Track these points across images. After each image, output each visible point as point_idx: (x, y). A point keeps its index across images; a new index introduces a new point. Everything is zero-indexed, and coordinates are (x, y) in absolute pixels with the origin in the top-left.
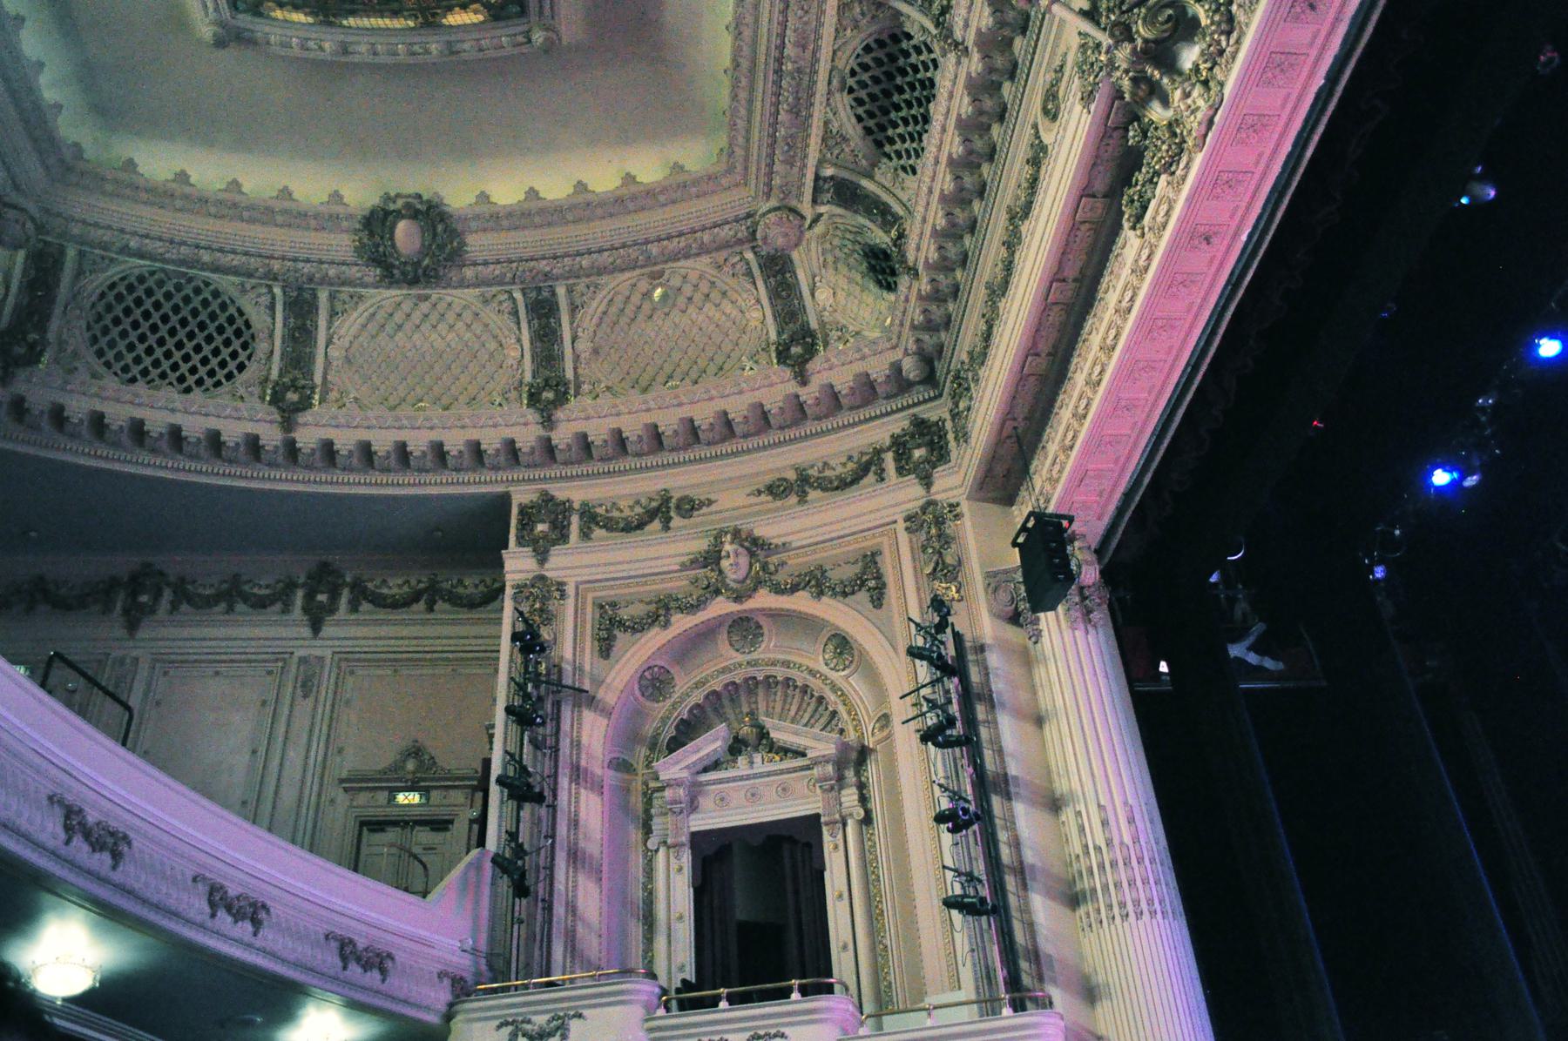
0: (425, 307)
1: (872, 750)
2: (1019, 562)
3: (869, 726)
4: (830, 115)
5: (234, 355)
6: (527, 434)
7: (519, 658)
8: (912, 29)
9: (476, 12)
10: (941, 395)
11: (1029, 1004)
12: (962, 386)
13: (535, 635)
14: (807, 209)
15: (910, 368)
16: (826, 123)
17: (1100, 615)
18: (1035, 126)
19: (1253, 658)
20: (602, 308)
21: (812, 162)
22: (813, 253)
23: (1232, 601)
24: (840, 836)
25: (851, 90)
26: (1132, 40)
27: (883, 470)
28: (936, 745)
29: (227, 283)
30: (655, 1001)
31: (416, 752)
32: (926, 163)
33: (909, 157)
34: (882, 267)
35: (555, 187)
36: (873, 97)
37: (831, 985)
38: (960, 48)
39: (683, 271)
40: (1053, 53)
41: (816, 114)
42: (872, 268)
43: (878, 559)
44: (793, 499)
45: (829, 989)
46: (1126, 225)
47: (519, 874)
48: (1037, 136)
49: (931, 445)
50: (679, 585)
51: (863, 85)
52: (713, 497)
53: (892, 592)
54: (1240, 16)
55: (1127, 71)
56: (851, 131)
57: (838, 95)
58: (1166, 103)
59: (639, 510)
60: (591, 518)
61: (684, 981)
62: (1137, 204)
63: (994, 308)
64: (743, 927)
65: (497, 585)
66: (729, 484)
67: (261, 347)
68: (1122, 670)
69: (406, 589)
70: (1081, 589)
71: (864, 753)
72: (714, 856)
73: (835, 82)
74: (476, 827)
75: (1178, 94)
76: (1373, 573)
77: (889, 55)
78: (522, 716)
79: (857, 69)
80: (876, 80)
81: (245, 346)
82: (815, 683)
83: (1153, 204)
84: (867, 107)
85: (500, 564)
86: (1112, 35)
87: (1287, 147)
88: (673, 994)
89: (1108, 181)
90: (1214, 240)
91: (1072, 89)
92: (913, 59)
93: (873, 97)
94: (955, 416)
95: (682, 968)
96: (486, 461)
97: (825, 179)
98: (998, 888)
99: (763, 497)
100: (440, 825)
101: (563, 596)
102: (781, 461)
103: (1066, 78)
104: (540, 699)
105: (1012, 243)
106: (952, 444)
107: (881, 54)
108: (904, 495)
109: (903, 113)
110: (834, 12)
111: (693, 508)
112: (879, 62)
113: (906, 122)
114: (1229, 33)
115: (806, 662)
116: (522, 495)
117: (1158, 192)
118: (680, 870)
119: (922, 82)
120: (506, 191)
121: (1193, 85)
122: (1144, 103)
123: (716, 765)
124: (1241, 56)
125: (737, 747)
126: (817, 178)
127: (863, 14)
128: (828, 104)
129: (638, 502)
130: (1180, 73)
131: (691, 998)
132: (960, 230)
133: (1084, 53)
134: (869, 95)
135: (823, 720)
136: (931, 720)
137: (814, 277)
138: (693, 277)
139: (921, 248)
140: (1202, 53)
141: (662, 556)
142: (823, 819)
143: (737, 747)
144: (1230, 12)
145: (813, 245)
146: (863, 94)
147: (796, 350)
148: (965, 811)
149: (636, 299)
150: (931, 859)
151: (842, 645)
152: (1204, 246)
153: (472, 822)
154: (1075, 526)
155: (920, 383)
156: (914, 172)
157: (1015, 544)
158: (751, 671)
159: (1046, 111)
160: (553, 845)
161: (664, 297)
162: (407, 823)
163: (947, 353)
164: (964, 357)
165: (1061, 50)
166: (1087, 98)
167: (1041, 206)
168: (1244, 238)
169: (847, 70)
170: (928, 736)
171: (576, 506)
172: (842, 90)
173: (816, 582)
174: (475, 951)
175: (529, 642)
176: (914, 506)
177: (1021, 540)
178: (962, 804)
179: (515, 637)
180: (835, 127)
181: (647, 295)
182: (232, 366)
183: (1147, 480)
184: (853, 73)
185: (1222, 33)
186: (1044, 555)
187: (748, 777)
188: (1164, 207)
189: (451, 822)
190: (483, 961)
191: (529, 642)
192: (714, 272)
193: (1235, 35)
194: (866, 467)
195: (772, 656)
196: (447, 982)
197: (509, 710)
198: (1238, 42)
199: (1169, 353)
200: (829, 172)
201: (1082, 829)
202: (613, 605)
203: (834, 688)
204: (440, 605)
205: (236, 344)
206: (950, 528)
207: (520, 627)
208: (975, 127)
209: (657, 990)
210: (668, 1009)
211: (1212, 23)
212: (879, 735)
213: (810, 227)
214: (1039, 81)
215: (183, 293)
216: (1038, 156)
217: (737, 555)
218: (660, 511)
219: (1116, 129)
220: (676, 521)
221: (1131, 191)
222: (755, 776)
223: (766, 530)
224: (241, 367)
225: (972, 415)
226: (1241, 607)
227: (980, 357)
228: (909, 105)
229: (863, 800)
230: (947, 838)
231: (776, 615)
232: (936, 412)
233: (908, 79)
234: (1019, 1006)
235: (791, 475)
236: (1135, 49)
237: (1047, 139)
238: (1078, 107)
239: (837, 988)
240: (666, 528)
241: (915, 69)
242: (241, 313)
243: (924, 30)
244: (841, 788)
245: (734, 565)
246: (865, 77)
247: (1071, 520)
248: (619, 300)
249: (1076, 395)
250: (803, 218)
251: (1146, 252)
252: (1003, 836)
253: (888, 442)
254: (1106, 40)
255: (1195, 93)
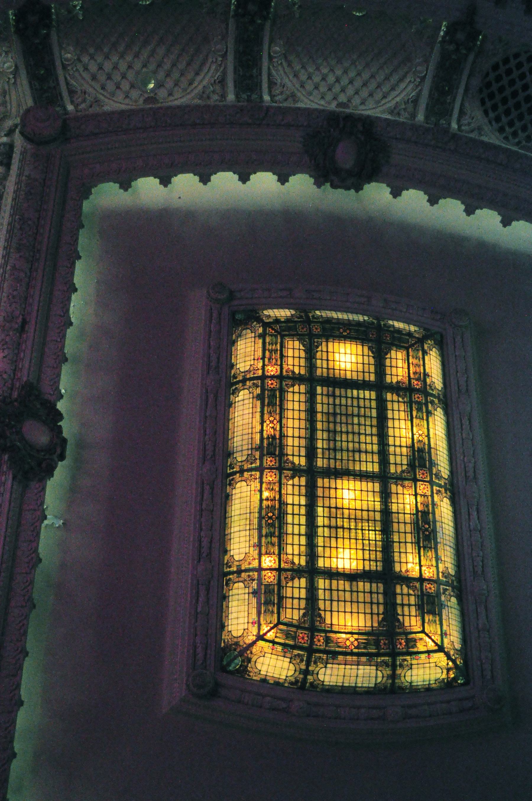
0: (342, 98)
5: (498, 79)
9: (269, 316)
20: (394, 94)
22: (14, 104)
29: (21, 111)
39: (127, 101)
67: (476, 82)
81: (488, 85)
137: (15, 83)
138: (120, 96)
145: (14, 110)
149: (169, 83)
181: (159, 85)
182: (502, 69)
205: (495, 87)
215: (513, 129)
224: (496, 67)
242: (486, 113)
248: (378, 95)
250: (22, 133)
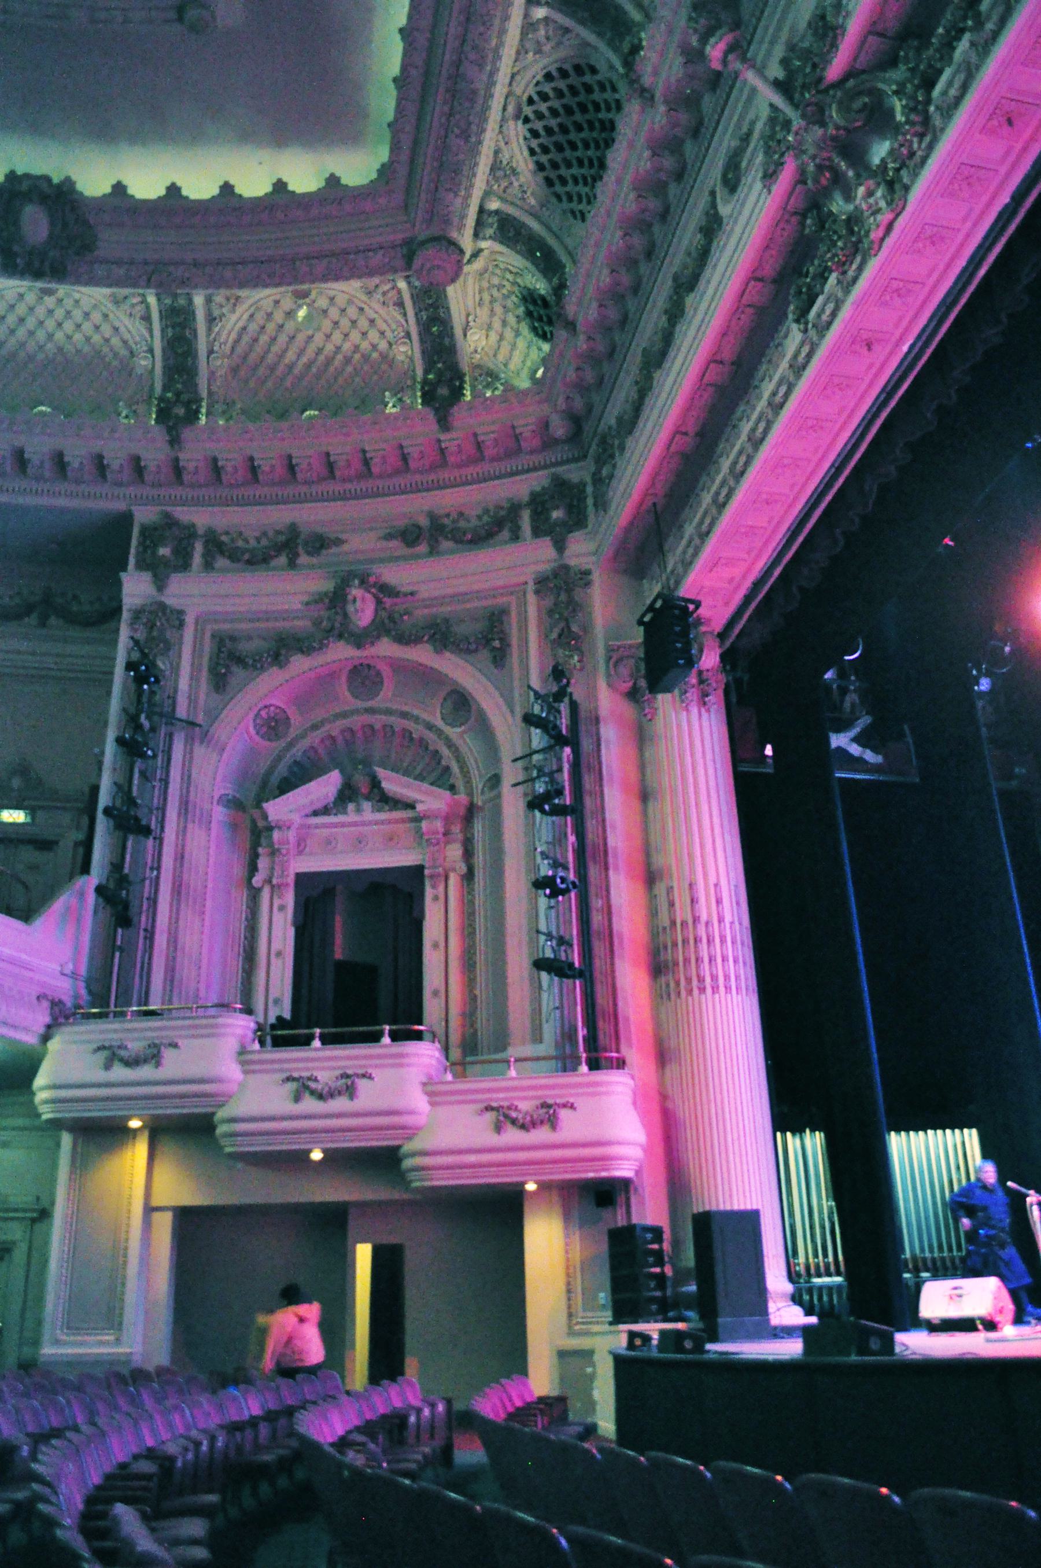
0: (50, 301)
1: (481, 809)
2: (641, 640)
3: (478, 783)
4: (502, 144)
6: (155, 453)
7: (133, 687)
8: (602, 66)
10: (585, 457)
11: (603, 1063)
12: (610, 452)
13: (152, 666)
14: (467, 243)
15: (559, 429)
16: (497, 152)
17: (716, 699)
18: (713, 193)
19: (855, 750)
21: (477, 194)
23: (844, 691)
24: (441, 888)
25: (526, 120)
26: (823, 124)
27: (519, 528)
28: (543, 812)
30: (250, 1035)
31: (23, 770)
32: (597, 212)
33: (580, 201)
34: (542, 314)
35: (200, 186)
36: (549, 131)
37: (421, 1032)
38: (646, 95)
40: (741, 118)
41: (486, 143)
42: (529, 314)
43: (505, 618)
44: (423, 548)
45: (418, 1036)
46: (791, 316)
47: (121, 907)
48: (714, 205)
49: (569, 508)
50: (302, 625)
51: (540, 116)
52: (343, 536)
53: (514, 659)
54: (937, 121)
55: (814, 157)
56: (522, 164)
57: (511, 123)
58: (849, 198)
59: (264, 542)
60: (218, 547)
61: (280, 1019)
62: (804, 297)
63: (649, 378)
64: (340, 965)
65: (114, 604)
66: (359, 523)
68: (729, 755)
69: (17, 600)
70: (700, 673)
71: (470, 812)
72: (316, 896)
73: (511, 109)
74: (81, 850)
75: (861, 190)
76: (978, 684)
77: (571, 88)
78: (131, 747)
79: (536, 98)
80: (554, 112)
82: (430, 736)
83: (820, 300)
84: (541, 140)
85: (118, 584)
86: (803, 116)
87: (962, 263)
88: (268, 1029)
89: (778, 267)
90: (876, 347)
91: (756, 160)
92: (597, 96)
93: (549, 131)
94: (598, 480)
95: (277, 1001)
96: (109, 476)
97: (490, 213)
98: (587, 952)
99: (394, 543)
100: (45, 845)
101: (181, 625)
102: (415, 507)
103: (752, 145)
104: (153, 729)
105: (675, 313)
106: (591, 509)
107: (562, 85)
108: (534, 556)
109: (579, 153)
110: (518, 32)
111: (322, 547)
112: (560, 94)
113: (581, 163)
114: (921, 136)
115: (424, 716)
116: (144, 515)
117: (827, 288)
118: (282, 908)
119: (602, 122)
120: (146, 184)
121: (878, 184)
122: (826, 193)
123: (325, 811)
124: (932, 164)
125: (347, 795)
126: (481, 210)
127: (548, 38)
128: (501, 132)
129: (265, 534)
130: (867, 167)
131: (283, 1035)
132: (624, 297)
133: (773, 128)
134: (550, 109)
135: (435, 774)
136: (540, 788)
137: (468, 315)
139: (582, 303)
140: (891, 152)
141: (284, 594)
142: (426, 872)
143: (347, 795)
144: (927, 111)
146: (539, 126)
147: (443, 391)
148: (563, 880)
150: (527, 920)
151: (461, 704)
152: (864, 351)
153: (77, 844)
154: (700, 611)
155: (564, 442)
156: (583, 220)
157: (640, 622)
158: (369, 719)
159: (725, 181)
160: (158, 877)
161: (308, 317)
162: (11, 841)
163: (596, 412)
164: (613, 422)
165: (751, 116)
166: (769, 176)
167: (709, 282)
168: (905, 348)
169: (525, 98)
170: (535, 803)
171: (200, 532)
172: (517, 117)
173: (441, 635)
174: (75, 975)
175: (143, 672)
176: (546, 568)
177: (646, 619)
178: (561, 873)
179: (130, 666)
180: (505, 157)
181: (290, 314)
183: (777, 573)
184: (531, 101)
185: (915, 134)
186: (664, 647)
187: (355, 824)
188: (831, 306)
189: (56, 843)
190: (83, 984)
191: (143, 672)
192: (364, 298)
193: (927, 139)
194: (498, 526)
195: (388, 705)
196: (46, 1004)
197: (120, 741)
198: (931, 147)
199: (816, 450)
200: (494, 205)
201: (672, 904)
202: (233, 639)
203: (450, 744)
204: (53, 620)
206: (578, 594)
207: (136, 656)
208: (653, 187)
209: (253, 1025)
210: (262, 1043)
211: (907, 122)
212: (489, 795)
213: (469, 262)
214: (724, 142)
216: (712, 226)
217: (363, 599)
218: (289, 547)
219: (795, 213)
220: (303, 559)
221: (801, 281)
222: (363, 824)
223: (394, 575)
225: (614, 483)
226: (851, 698)
227: (629, 423)
228: (587, 146)
229: (468, 854)
230: (543, 902)
231: (399, 667)
232: (577, 473)
233: (587, 117)
234: (594, 1065)
235: (424, 522)
236: (825, 135)
237: (724, 210)
238: (758, 185)
239: (426, 1035)
240: (292, 564)
241: (597, 108)
243: (612, 67)
244: (447, 843)
245: (363, 610)
246: (543, 107)
247: (698, 604)
248: (260, 317)
249: (719, 479)
250: (462, 252)
251: (805, 350)
252: (596, 903)
253: (526, 499)
254: (797, 122)
255: (879, 193)
